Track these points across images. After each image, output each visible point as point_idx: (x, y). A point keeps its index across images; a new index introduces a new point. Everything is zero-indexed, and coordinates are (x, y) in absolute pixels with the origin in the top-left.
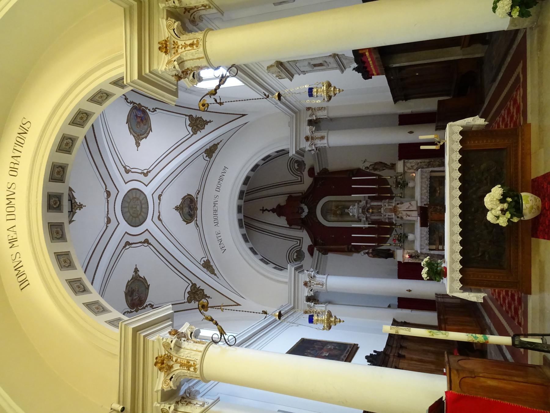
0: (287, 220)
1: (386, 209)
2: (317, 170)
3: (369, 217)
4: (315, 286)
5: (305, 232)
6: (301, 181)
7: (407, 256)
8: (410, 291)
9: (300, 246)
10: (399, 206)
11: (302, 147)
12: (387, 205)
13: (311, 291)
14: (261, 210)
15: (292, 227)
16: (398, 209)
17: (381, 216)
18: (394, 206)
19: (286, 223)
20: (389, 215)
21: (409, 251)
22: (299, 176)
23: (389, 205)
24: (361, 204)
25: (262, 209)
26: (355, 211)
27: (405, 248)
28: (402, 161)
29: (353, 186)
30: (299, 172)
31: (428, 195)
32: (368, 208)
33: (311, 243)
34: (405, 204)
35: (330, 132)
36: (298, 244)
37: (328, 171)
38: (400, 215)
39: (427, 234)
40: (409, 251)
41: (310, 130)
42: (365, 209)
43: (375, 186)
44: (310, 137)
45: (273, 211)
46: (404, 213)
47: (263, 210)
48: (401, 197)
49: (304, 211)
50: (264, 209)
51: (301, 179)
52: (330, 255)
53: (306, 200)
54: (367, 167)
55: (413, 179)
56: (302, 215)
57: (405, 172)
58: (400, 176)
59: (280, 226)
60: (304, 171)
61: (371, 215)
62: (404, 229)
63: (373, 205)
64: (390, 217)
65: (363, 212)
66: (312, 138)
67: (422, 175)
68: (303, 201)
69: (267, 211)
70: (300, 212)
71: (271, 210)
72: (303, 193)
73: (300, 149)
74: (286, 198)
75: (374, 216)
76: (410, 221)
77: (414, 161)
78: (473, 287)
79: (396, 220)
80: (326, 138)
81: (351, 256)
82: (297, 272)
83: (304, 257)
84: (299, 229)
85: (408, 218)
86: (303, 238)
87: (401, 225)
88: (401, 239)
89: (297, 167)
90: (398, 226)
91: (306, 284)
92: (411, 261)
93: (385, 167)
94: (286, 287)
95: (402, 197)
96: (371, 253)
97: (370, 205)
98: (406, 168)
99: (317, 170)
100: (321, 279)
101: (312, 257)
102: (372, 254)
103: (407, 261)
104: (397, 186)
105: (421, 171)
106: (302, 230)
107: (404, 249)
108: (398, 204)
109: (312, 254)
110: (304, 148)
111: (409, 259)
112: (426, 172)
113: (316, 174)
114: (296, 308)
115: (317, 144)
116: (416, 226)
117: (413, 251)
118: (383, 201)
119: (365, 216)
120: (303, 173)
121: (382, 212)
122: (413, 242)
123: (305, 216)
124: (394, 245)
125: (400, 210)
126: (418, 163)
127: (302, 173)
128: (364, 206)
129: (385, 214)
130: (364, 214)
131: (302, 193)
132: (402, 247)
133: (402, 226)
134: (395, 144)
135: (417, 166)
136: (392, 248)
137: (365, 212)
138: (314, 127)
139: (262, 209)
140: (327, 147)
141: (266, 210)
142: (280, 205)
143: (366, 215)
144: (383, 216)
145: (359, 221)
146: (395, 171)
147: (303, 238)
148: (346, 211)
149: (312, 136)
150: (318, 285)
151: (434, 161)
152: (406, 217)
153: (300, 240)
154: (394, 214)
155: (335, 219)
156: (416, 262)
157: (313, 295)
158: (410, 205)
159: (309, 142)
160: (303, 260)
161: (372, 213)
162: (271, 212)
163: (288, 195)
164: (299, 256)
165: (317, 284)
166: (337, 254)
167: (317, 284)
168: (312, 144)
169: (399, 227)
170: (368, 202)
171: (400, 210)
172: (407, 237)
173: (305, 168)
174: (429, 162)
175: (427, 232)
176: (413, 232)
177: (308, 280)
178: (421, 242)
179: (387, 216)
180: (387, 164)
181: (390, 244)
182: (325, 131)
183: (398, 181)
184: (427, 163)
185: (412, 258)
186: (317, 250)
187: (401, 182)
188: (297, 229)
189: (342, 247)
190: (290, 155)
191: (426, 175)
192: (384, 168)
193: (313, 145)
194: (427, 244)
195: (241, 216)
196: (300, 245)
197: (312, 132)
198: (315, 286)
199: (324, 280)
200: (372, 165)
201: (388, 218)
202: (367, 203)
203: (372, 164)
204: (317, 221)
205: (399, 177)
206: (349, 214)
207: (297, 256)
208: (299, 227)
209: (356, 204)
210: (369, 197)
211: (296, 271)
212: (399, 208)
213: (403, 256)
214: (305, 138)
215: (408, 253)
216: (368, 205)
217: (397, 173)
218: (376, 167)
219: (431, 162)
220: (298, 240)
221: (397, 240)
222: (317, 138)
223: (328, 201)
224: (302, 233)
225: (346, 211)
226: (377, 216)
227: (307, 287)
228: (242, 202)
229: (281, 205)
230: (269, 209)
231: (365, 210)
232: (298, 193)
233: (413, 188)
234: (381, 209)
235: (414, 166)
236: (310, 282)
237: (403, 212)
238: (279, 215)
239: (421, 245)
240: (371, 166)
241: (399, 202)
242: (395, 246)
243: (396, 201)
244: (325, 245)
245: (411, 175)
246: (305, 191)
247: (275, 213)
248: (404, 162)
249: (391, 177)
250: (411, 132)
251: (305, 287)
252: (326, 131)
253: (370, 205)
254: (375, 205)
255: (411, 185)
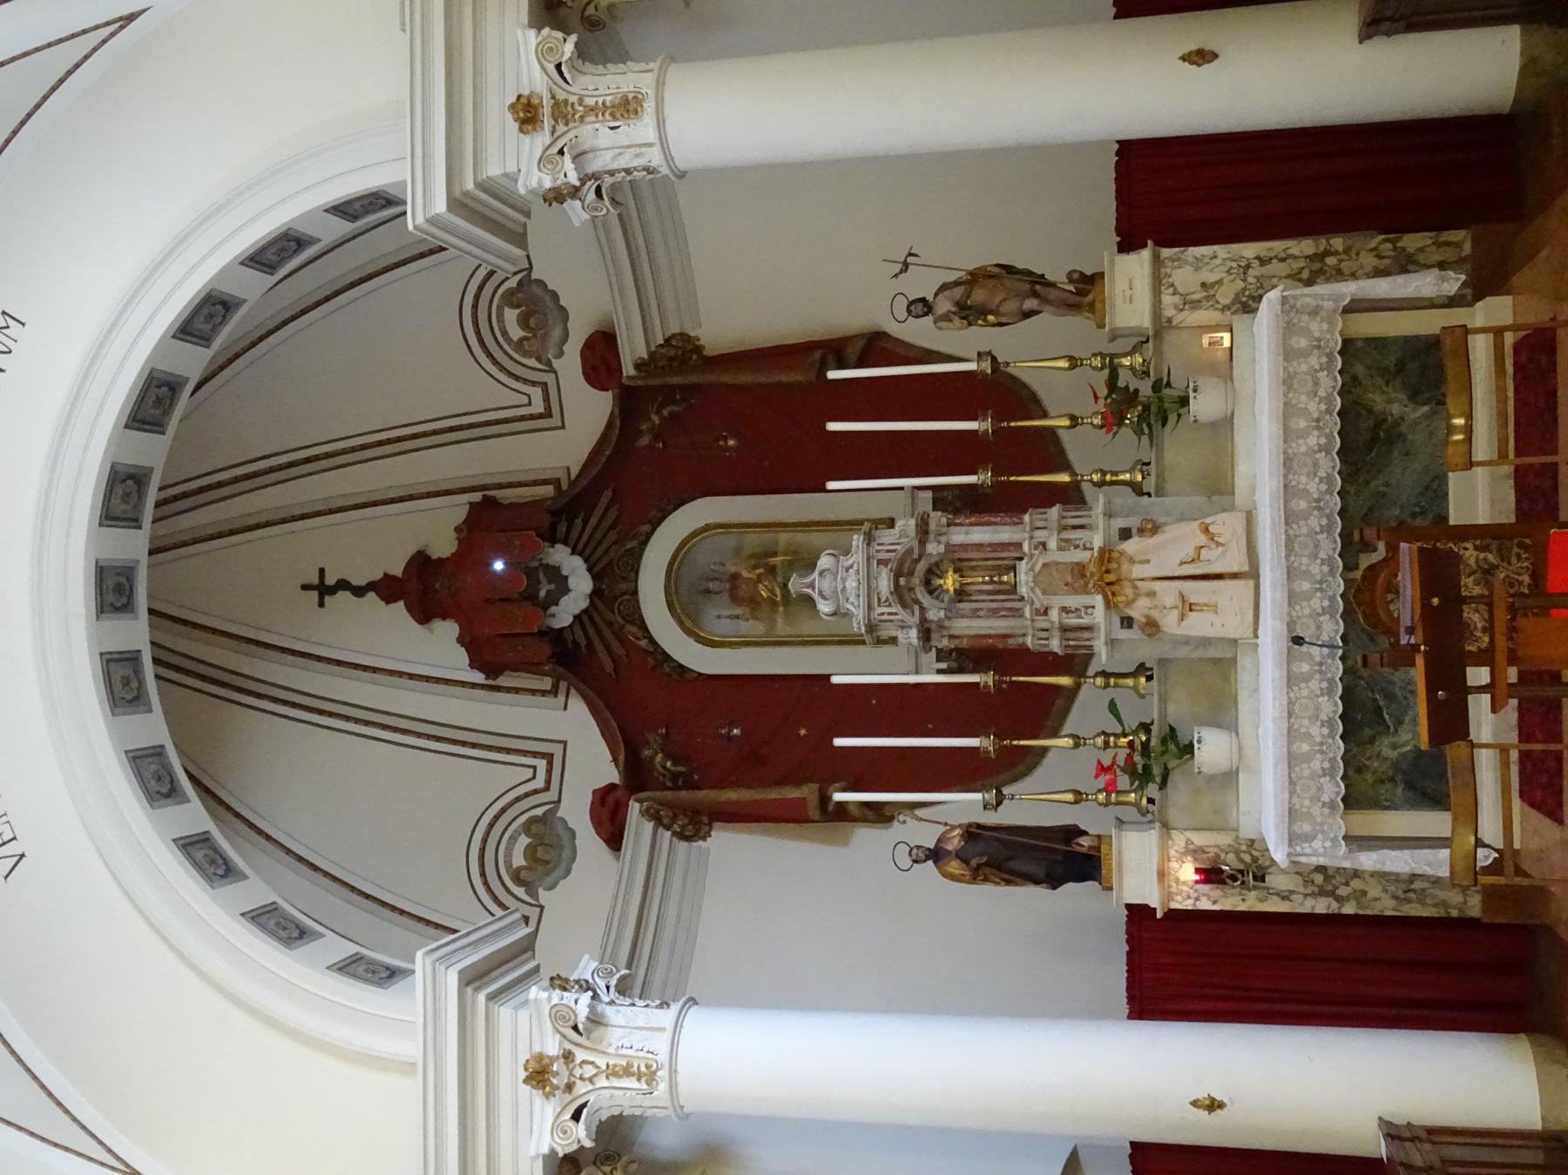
0: (468, 641)
1: (1045, 565)
2: (632, 349)
3: (941, 626)
4: (602, 1082)
5: (578, 707)
6: (548, 414)
7: (1187, 872)
8: (1213, 1105)
9: (551, 795)
10: (1131, 546)
11: (493, 170)
12: (1052, 544)
13: (576, 1117)
14: (305, 587)
15: (503, 681)
16: (1125, 567)
17: (1016, 613)
18: (1102, 551)
19: (462, 656)
20: (1065, 610)
21: (1199, 839)
22: (534, 384)
23: (1065, 545)
24: (886, 537)
25: (316, 581)
26: (851, 584)
27: (1174, 815)
28: (1146, 254)
29: (833, 426)
30: (532, 362)
31: (1330, 465)
32: (937, 564)
33: (612, 775)
34: (1170, 532)
35: (675, 73)
36: (539, 782)
37: (698, 349)
38: (1138, 611)
39: (1331, 735)
40: (1199, 839)
41: (542, 52)
42: (911, 573)
43: (973, 418)
44: (547, 104)
45: (388, 589)
46: (1168, 593)
47: (324, 590)
48: (1138, 489)
49: (567, 590)
50: (330, 580)
51: (547, 399)
52: (724, 842)
53: (579, 522)
54: (923, 300)
55: (1225, 369)
56: (553, 609)
57: (1162, 326)
58: (1131, 353)
59: (427, 679)
60: (560, 354)
61: (951, 614)
62: (1163, 700)
63: (964, 547)
64: (1072, 621)
65: (901, 594)
66: (562, 112)
67: (1288, 329)
68: (562, 528)
69: (344, 596)
70: (542, 593)
71: (372, 586)
72: (565, 486)
73: (481, 186)
74: (461, 514)
75: (975, 614)
76: (1205, 642)
77: (1221, 250)
78: (1386, 906)
79: (1112, 643)
80: (649, 106)
81: (845, 842)
82: (481, 997)
83: (574, 859)
84: (544, 693)
85: (1197, 625)
86: (565, 743)
87: (1142, 669)
88: (1146, 768)
89: (516, 333)
90: (1125, 676)
91: (539, 1075)
92: (1210, 900)
93: (1035, 294)
94: (411, 1087)
95: (1149, 485)
96: (960, 856)
97: (948, 545)
98: (1168, 299)
99: (632, 349)
100: (637, 1039)
101: (618, 859)
102: (966, 862)
103: (1188, 905)
104: (1114, 420)
105: (1284, 300)
106: (561, 698)
107: (1166, 826)
108: (1125, 534)
109: (614, 839)
110: (506, 175)
111: (1206, 888)
112: (1314, 312)
113: (628, 369)
114: (637, 991)
115: (593, 150)
116: (1244, 677)
117: (1225, 839)
118: (1027, 518)
119: (916, 619)
120: (556, 363)
121: (1023, 590)
122: (1229, 778)
123: (577, 618)
124: (1101, 797)
125: (1138, 571)
126: (1248, 266)
127: (549, 363)
128: (909, 551)
129: (1040, 600)
130: (904, 605)
131: (556, 482)
132: (1155, 816)
133: (1149, 678)
134: (1100, 144)
135: (1241, 285)
136: (1089, 819)
137: (911, 589)
138: (573, 38)
139: (316, 581)
140: (665, 170)
141: (343, 585)
142: (428, 559)
143: (922, 609)
144: (1027, 613)
145: (875, 636)
146: (1101, 326)
147: (565, 743)
148: (796, 584)
149: (561, 96)
150: (615, 1074)
151: (1347, 251)
152: (1182, 618)
153: (551, 757)
154: (1098, 600)
155: (754, 628)
156: (1242, 907)
157: (588, 1144)
158: (1202, 540)
159: (541, 139)
160: (568, 872)
161: (961, 594)
162: (372, 595)
163: (477, 497)
164: (540, 852)
165: (612, 1072)
166: (751, 832)
167: (612, 1072)
168: (561, 152)
169: (1130, 682)
170: (932, 526)
171: (1138, 571)
172: (1188, 749)
173: (565, 337)
174: (1320, 257)
175: (1329, 723)
176: (1223, 713)
177: (552, 1047)
178: (1292, 793)
179: (1054, 615)
180: (1050, 277)
181: (1077, 793)
182: (643, 66)
183: (1121, 384)
184: (1302, 263)
185: (1223, 882)
186: (648, 814)
187: (1145, 388)
188: (533, 692)
189: (791, 793)
190: (415, 219)
191: (1317, 327)
192: (1030, 304)
193: (567, 157)
194: (1332, 806)
195: (135, 633)
196: (547, 788)
197: (558, 67)
198: (602, 1082)
199: (661, 1044)
200: (956, 284)
201: (1065, 629)
202: (923, 531)
203: (952, 277)
204: (643, 643)
205: (1126, 361)
206: (810, 601)
207: (530, 852)
208: (547, 683)
209: (857, 540)
210: (942, 498)
211: (477, 990)
212: (1132, 561)
213: (1162, 874)
214: (513, 107)
215: (1194, 852)
216: (934, 549)
217: (1114, 336)
218: (979, 296)
219: (1327, 253)
220: (535, 754)
221: (1123, 770)
222: (592, 109)
223: (707, 528)
224: (561, 713)
225: (796, 584)
226: (994, 613)
227: (547, 1096)
228: (132, 545)
229: (434, 557)
230: (359, 580)
231: (916, 581)
232: (535, 483)
233: (1224, 426)
234: (1014, 568)
235: (1220, 282)
236: (568, 1056)
237: (1158, 586)
238: (424, 613)
239: (1293, 814)
240: (941, 296)
241: (1132, 522)
242: (1107, 804)
243: (1109, 514)
244: (692, 786)
245: (1205, 340)
246: (575, 471)
247: (401, 604)
248: (1157, 261)
249: (1074, 362)
250: (1201, 57)
251: (537, 1096)
252: (652, 65)
253: (948, 545)
254: (979, 546)
255: (1205, 405)
